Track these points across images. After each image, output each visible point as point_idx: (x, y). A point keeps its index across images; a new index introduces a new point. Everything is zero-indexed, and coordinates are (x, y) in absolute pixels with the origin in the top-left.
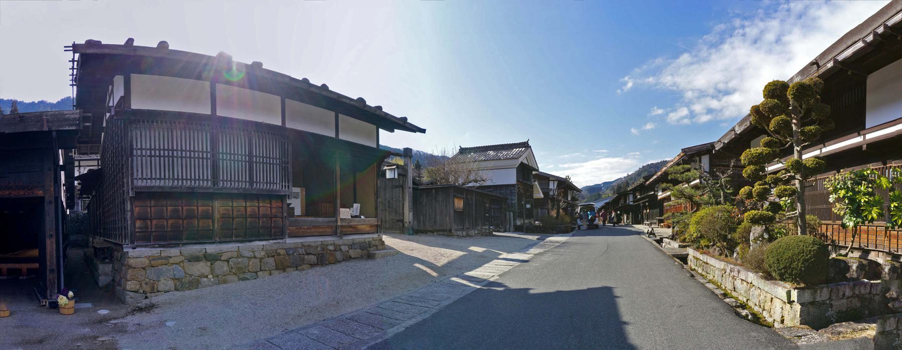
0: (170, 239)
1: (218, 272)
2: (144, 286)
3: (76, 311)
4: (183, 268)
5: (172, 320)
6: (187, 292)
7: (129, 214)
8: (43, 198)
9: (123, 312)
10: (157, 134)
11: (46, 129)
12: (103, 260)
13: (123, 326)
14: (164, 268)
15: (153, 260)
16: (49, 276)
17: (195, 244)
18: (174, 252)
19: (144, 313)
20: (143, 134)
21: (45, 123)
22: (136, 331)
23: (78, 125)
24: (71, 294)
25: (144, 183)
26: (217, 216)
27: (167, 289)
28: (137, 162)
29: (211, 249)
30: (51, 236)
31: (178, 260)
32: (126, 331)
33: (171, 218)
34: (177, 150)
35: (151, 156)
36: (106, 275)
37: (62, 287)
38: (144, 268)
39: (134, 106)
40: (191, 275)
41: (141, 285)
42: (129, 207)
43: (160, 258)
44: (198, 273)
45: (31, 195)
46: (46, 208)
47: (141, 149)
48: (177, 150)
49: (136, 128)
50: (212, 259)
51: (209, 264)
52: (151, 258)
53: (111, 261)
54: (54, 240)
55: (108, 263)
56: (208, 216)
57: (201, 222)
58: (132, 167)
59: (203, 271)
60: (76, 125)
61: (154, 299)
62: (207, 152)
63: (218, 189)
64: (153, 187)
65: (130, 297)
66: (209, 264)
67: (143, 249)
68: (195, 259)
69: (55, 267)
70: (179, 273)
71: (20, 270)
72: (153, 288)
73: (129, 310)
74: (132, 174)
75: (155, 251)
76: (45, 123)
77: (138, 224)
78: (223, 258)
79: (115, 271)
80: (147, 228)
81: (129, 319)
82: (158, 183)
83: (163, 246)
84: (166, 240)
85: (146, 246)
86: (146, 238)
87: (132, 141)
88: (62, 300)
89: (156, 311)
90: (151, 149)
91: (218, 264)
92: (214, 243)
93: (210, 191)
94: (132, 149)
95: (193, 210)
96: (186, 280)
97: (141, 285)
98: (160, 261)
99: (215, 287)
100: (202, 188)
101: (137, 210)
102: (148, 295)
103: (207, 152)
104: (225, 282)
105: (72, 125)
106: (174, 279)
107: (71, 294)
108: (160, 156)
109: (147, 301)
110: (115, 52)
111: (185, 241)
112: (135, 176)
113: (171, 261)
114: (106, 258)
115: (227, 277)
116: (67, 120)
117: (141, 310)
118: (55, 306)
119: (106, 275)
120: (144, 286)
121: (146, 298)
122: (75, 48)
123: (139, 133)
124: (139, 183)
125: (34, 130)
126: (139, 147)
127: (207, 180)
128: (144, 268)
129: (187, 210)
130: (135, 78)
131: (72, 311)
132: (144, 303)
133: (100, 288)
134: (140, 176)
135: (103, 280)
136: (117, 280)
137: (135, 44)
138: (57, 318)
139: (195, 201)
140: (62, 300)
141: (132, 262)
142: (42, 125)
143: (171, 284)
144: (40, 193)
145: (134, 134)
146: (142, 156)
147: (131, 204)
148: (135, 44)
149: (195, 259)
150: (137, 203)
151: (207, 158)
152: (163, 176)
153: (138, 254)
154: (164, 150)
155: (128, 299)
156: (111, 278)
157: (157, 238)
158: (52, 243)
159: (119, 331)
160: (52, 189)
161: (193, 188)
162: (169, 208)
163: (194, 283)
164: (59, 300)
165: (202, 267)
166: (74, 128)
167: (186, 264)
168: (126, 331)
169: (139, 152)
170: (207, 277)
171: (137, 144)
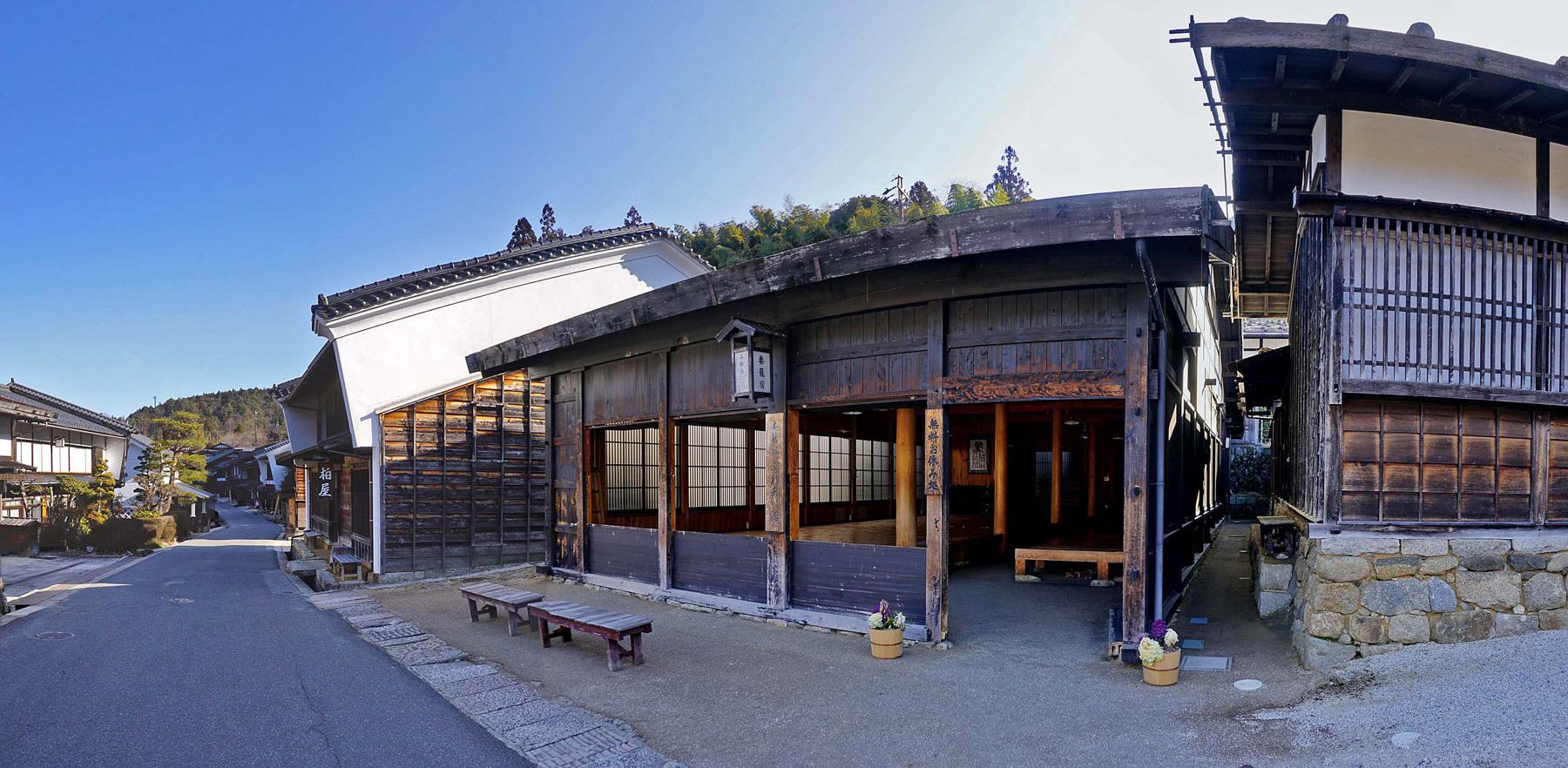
0: (1426, 514)
1: (1537, 599)
2: (1354, 625)
3: (1183, 676)
4: (1453, 584)
5: (1411, 728)
6: (1462, 647)
7: (1328, 447)
8: (1120, 403)
9: (1293, 689)
10: (1403, 255)
11: (1119, 235)
12: (1272, 555)
13: (1285, 733)
14: (1407, 583)
15: (1382, 562)
16: (1128, 588)
17: (1487, 527)
18: (1433, 545)
19: (1346, 698)
20: (1369, 253)
21: (1118, 220)
22: (1314, 751)
23: (1198, 224)
24: (1171, 636)
25: (1366, 374)
26: (1542, 461)
27: (1410, 636)
28: (1352, 321)
29: (1525, 542)
30: (1137, 492)
31: (1442, 565)
32: (1287, 750)
33: (1431, 462)
34: (1450, 297)
35: (1386, 308)
36: (1276, 588)
37: (1159, 615)
38: (1357, 583)
39: (1348, 190)
40: (1471, 605)
41: (1346, 623)
42: (1327, 429)
43: (1400, 559)
44: (1489, 601)
45: (1094, 395)
46: (1128, 426)
47: (1363, 290)
48: (1450, 297)
49: (1352, 238)
50: (1514, 562)
51: (1518, 578)
52: (1378, 559)
53: (1292, 559)
54: (1142, 502)
55: (1283, 561)
56: (1520, 462)
57: (1504, 474)
58: (1338, 334)
59: (1503, 596)
60: (1193, 224)
61: (1378, 661)
62: (1524, 306)
63: (1549, 397)
64: (1388, 384)
65: (1315, 651)
66: (1518, 578)
67: (1358, 535)
68: (1482, 566)
69: (1141, 568)
70: (1444, 601)
71: (1093, 566)
72: (1375, 632)
73: (1312, 686)
74: (1338, 349)
75: (1388, 543)
76: (1118, 220)
77: (1350, 472)
78: (1551, 566)
79: (1295, 580)
80: (1370, 483)
81: (1307, 708)
82: (1399, 375)
83: (1408, 530)
84: (1414, 515)
85: (1366, 528)
86: (1369, 507)
87: (1340, 267)
88: (1149, 649)
89: (1378, 693)
90: (1386, 292)
91: (1539, 577)
92: (1532, 527)
93: (1530, 400)
94: (1339, 289)
95: (1485, 446)
96: (1460, 616)
97: (1346, 623)
98: (1397, 567)
99: (1529, 637)
100: (1510, 392)
101: (1347, 439)
102: (1364, 649)
103: (1524, 306)
104: (1554, 625)
105: (1183, 226)
106: (1430, 612)
107: (1171, 636)
108: (1408, 310)
109: (1358, 666)
110: (1295, 43)
111: (1461, 521)
112: (1344, 355)
113: (1426, 567)
114: (1282, 550)
115: (1561, 614)
116: (1170, 212)
117: (1339, 686)
118: (1132, 659)
119: (1276, 588)
120: (1354, 625)
121: (1358, 655)
122: (1197, 34)
123: (1358, 253)
124: (1355, 374)
125: (1093, 237)
126: (1358, 284)
127: (1522, 373)
128: (1357, 583)
129: (1472, 445)
130: (1350, 118)
131: (1172, 677)
132: (1350, 669)
133: (1264, 620)
134: (1357, 356)
135: (1268, 602)
136: (1298, 603)
137: (1350, 25)
138: (1128, 690)
139: (1492, 424)
140: (1149, 649)
141: (1326, 565)
142: (1111, 225)
143: (1421, 624)
144: (1114, 390)
145: (1346, 253)
146: (1364, 307)
147: (1334, 423)
148: (1350, 25)
149: (1482, 566)
150: (1349, 422)
151: (1524, 321)
152: (1413, 360)
153: (1340, 547)
154: (1419, 294)
155: (1313, 656)
156: (1288, 598)
157: (1394, 510)
158: (1137, 508)
159: (1270, 749)
160: (1144, 381)
161: (1487, 392)
162: (1426, 437)
163: (1479, 626)
164: (1141, 649)
165: (1503, 586)
166: (1188, 232)
167: (1462, 576)
168: (1287, 750)
169: (1357, 296)
170: (1511, 609)
171: (1353, 278)
